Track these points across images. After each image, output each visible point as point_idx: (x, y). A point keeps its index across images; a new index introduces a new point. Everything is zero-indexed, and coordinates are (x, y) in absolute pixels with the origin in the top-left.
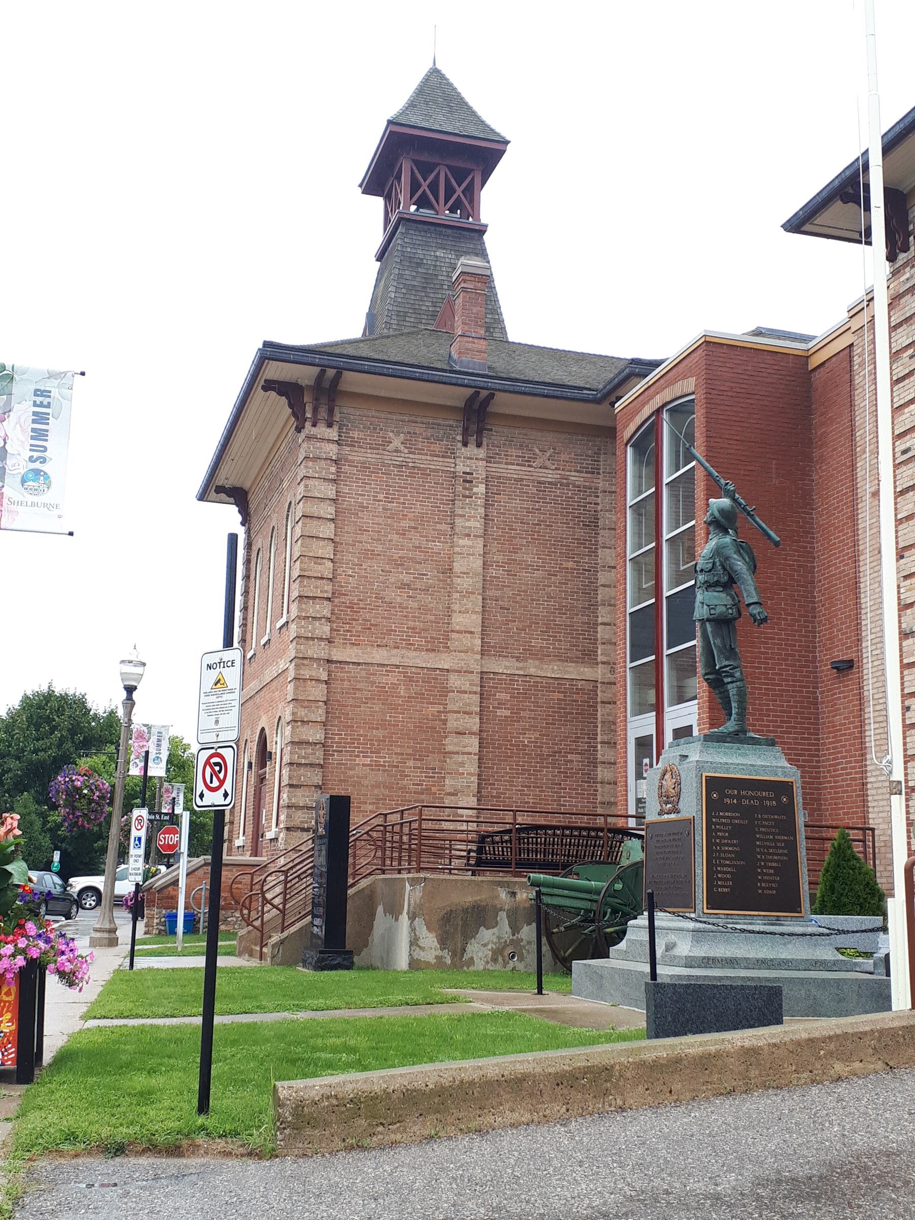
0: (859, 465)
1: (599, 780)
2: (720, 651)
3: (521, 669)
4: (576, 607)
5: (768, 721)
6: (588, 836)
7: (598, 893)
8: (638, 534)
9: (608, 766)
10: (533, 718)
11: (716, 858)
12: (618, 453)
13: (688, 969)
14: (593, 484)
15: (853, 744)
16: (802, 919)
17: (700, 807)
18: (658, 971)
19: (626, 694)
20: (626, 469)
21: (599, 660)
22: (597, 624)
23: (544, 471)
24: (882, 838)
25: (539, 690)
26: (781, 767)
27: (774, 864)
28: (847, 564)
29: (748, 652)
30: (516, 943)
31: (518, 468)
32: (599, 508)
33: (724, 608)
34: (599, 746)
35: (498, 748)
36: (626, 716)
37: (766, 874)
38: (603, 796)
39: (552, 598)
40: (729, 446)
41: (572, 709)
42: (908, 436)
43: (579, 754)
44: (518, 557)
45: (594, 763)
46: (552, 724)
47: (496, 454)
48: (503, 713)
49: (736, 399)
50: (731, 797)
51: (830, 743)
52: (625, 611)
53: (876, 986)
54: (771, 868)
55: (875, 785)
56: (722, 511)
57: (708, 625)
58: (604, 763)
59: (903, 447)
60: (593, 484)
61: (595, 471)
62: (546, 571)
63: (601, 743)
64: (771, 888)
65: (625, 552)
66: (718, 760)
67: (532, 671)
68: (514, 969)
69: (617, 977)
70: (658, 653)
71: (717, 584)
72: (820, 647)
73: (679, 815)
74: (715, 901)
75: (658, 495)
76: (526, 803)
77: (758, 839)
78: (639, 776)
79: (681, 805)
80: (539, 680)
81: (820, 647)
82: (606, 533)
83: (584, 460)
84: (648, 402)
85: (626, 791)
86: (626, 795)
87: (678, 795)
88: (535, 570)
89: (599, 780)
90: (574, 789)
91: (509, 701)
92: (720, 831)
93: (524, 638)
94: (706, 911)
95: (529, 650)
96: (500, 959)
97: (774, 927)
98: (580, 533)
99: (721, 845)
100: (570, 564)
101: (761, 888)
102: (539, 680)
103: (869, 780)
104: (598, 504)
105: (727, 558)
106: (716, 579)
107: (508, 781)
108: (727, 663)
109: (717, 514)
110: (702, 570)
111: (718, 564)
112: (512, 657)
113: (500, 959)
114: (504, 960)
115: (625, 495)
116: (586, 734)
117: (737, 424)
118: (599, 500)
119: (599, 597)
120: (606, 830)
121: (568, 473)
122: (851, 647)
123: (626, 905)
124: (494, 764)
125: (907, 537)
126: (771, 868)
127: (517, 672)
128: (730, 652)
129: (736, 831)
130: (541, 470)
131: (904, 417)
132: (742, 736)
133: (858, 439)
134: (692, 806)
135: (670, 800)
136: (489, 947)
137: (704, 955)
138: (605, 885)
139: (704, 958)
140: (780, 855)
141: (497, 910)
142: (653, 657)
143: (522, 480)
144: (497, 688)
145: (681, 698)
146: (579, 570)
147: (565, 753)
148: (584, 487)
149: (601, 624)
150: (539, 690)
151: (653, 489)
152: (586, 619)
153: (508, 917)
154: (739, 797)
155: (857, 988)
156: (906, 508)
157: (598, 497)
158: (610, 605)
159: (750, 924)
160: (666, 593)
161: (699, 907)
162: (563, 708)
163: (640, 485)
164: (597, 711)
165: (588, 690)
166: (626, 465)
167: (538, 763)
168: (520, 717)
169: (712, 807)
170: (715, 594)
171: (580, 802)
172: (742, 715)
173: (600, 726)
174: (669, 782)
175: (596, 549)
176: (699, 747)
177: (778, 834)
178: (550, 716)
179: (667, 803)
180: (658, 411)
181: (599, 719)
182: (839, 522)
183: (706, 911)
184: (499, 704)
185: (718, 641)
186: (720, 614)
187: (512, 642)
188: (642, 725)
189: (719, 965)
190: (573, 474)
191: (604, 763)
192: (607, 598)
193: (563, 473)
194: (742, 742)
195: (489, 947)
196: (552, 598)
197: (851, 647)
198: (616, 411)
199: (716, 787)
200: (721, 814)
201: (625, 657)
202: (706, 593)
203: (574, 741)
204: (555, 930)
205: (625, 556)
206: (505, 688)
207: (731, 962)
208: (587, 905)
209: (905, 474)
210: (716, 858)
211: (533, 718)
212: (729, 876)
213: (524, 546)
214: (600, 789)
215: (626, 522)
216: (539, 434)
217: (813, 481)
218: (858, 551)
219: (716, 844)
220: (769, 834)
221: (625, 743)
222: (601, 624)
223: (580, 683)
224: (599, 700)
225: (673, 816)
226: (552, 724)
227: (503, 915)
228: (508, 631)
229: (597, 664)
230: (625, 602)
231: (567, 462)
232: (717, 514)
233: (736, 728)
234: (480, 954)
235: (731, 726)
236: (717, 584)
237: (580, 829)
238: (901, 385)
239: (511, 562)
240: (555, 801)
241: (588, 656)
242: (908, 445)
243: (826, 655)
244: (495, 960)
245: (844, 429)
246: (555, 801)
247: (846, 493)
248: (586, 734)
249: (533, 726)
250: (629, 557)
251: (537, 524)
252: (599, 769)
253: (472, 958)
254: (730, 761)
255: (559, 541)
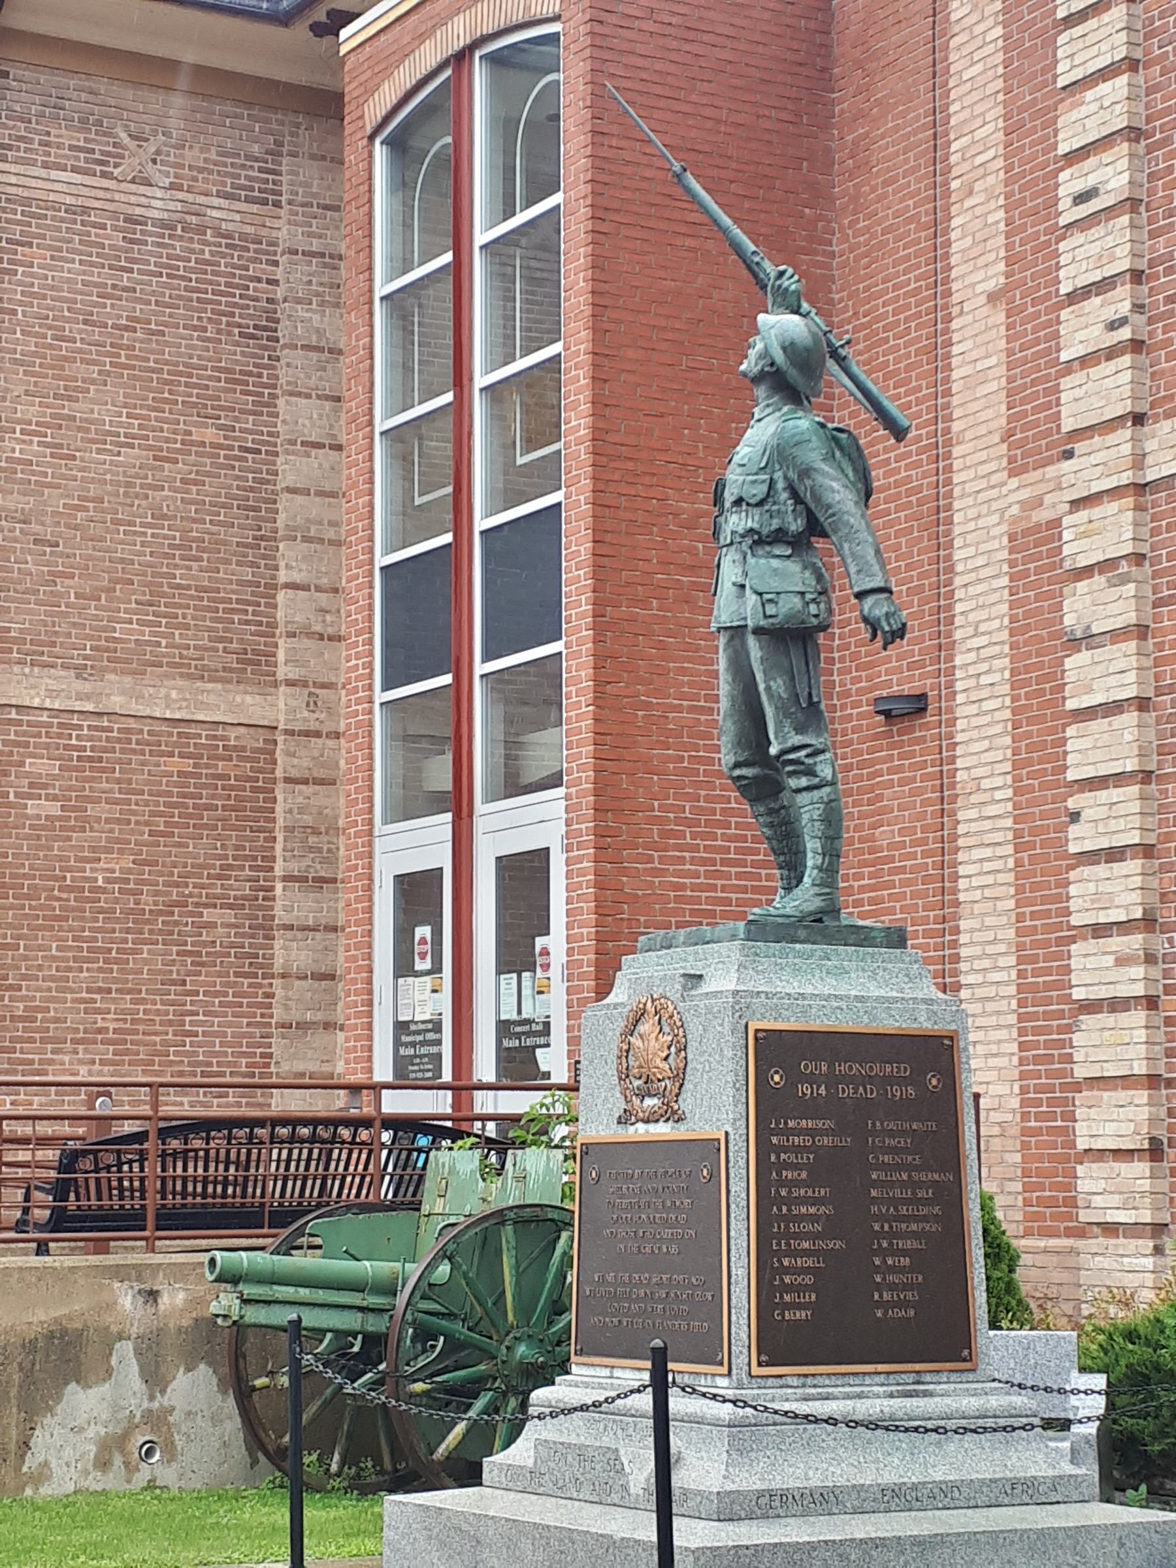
0: (955, 223)
1: (277, 968)
2: (783, 711)
3: (87, 697)
4: (225, 543)
5: (725, 837)
6: (313, 1139)
7: (390, 1289)
8: (403, 367)
9: (299, 935)
10: (118, 821)
11: (779, 1236)
12: (350, 158)
13: (730, 1527)
14: (264, 232)
15: (923, 895)
16: (971, 1376)
17: (741, 1108)
18: (677, 1542)
19: (371, 769)
20: (370, 201)
21: (280, 676)
22: (275, 587)
23: (142, 189)
24: (995, 1117)
25: (134, 751)
26: (925, 1001)
27: (909, 1244)
28: (918, 464)
29: (683, 671)
30: (156, 1419)
31: (77, 178)
32: (280, 292)
33: (797, 601)
34: (279, 887)
35: (28, 897)
36: (371, 822)
37: (893, 1269)
38: (287, 1008)
39: (164, 517)
40: (645, 160)
41: (213, 797)
42: (1092, 161)
43: (231, 907)
44: (78, 410)
45: (266, 928)
46: (163, 834)
47: (20, 139)
48: (41, 808)
49: (662, 41)
50: (812, 1079)
51: (862, 889)
52: (371, 562)
53: (1155, 1537)
54: (904, 1253)
55: (980, 992)
56: (789, 348)
57: (752, 642)
58: (290, 928)
59: (1079, 186)
60: (264, 232)
61: (268, 198)
62: (150, 448)
63: (285, 879)
64: (903, 1304)
65: (371, 412)
66: (782, 987)
67: (116, 702)
68: (151, 1486)
69: (526, 1545)
70: (460, 668)
71: (779, 536)
72: (842, 659)
73: (682, 1127)
74: (780, 1346)
75: (458, 271)
76: (100, 1031)
77: (875, 1184)
78: (404, 967)
79: (686, 1103)
80: (133, 724)
81: (842, 659)
82: (298, 357)
83: (243, 167)
84: (429, 33)
85: (370, 1003)
86: (370, 1014)
87: (680, 1076)
88: (122, 445)
89: (277, 968)
90: (217, 994)
91: (55, 778)
92: (787, 1166)
93: (96, 618)
94: (756, 1370)
95: (107, 650)
96: (118, 1460)
97: (915, 1401)
98: (234, 354)
99: (790, 1201)
100: (210, 434)
101: (879, 1304)
102: (133, 724)
103: (964, 980)
104: (275, 283)
105: (806, 472)
106: (775, 524)
107: (53, 979)
108: (797, 740)
109: (779, 357)
110: (739, 502)
111: (780, 485)
112: (65, 667)
113: (118, 1460)
114: (127, 1464)
115: (370, 268)
116: (246, 858)
117: (662, 103)
118: (279, 273)
119: (282, 519)
120: (378, 1124)
121: (202, 199)
122: (920, 665)
123: (450, 1315)
124: (19, 937)
125: (1082, 406)
126: (904, 1253)
127: (78, 706)
128: (809, 713)
129: (826, 1168)
130: (133, 187)
131: (1084, 111)
132: (828, 921)
133: (953, 159)
134: (717, 1105)
135: (656, 1086)
136: (91, 1433)
137: (759, 1486)
138: (414, 1270)
139: (760, 1494)
140: (925, 1219)
141: (109, 1340)
142: (447, 679)
143: (86, 210)
144: (26, 745)
145: (513, 784)
146: (231, 448)
147: (197, 905)
148: (243, 237)
149: (287, 586)
150: (134, 751)
151: (448, 257)
152: (248, 574)
153: (138, 1353)
154: (833, 1081)
155: (1116, 1547)
156: (1081, 335)
157: (276, 263)
158: (307, 539)
159: (860, 1396)
160: (482, 523)
161: (740, 1361)
162: (192, 796)
163: (407, 243)
164: (275, 800)
165: (253, 751)
166: (370, 191)
167: (128, 931)
168: (86, 819)
169: (770, 1108)
170: (775, 563)
171: (230, 1025)
172: (829, 873)
173: (280, 837)
174: (651, 1041)
175: (273, 396)
176: (736, 956)
177: (917, 1168)
178: (161, 814)
179: (642, 1095)
180: (461, 58)
181: (280, 822)
182: (897, 361)
183: (756, 1370)
184: (31, 785)
185: (779, 685)
186: (789, 617)
187: (64, 628)
188: (424, 844)
189: (796, 1509)
190: (216, 201)
191: (290, 928)
192: (299, 520)
193: (189, 197)
194: (830, 938)
195: (91, 1433)
196: (164, 517)
197: (920, 665)
198: (344, 50)
199: (784, 1059)
200: (791, 1124)
201: (371, 676)
202: (751, 561)
203: (219, 877)
204: (258, 1383)
205: (371, 423)
206: (47, 746)
207: (821, 1501)
208: (351, 1321)
209: (1080, 253)
210: (779, 1236)
211: (118, 821)
212: (809, 1280)
213: (93, 382)
214: (279, 992)
215: (372, 336)
216: (130, 93)
217: (832, 255)
218: (947, 431)
219: (780, 1201)
220: (899, 1168)
221: (369, 888)
222: (287, 586)
223: (232, 733)
224: (279, 773)
225: (662, 1130)
226: (163, 834)
227: (125, 1351)
228: (54, 600)
229: (275, 684)
230: (371, 539)
231: (201, 170)
232: (779, 357)
233: (818, 903)
234: (68, 1453)
235: (804, 898)
236: (779, 536)
237: (314, 1122)
238: (1078, 31)
239: (60, 422)
240: (171, 1023)
241: (254, 667)
242: (1091, 181)
243: (859, 680)
244: (103, 1464)
245: (915, 133)
246: (171, 1023)
247: (917, 291)
248: (246, 858)
249: (118, 841)
250: (380, 425)
251: (126, 328)
252: (278, 944)
253: (46, 1464)
254: (809, 990)
255: (181, 374)
